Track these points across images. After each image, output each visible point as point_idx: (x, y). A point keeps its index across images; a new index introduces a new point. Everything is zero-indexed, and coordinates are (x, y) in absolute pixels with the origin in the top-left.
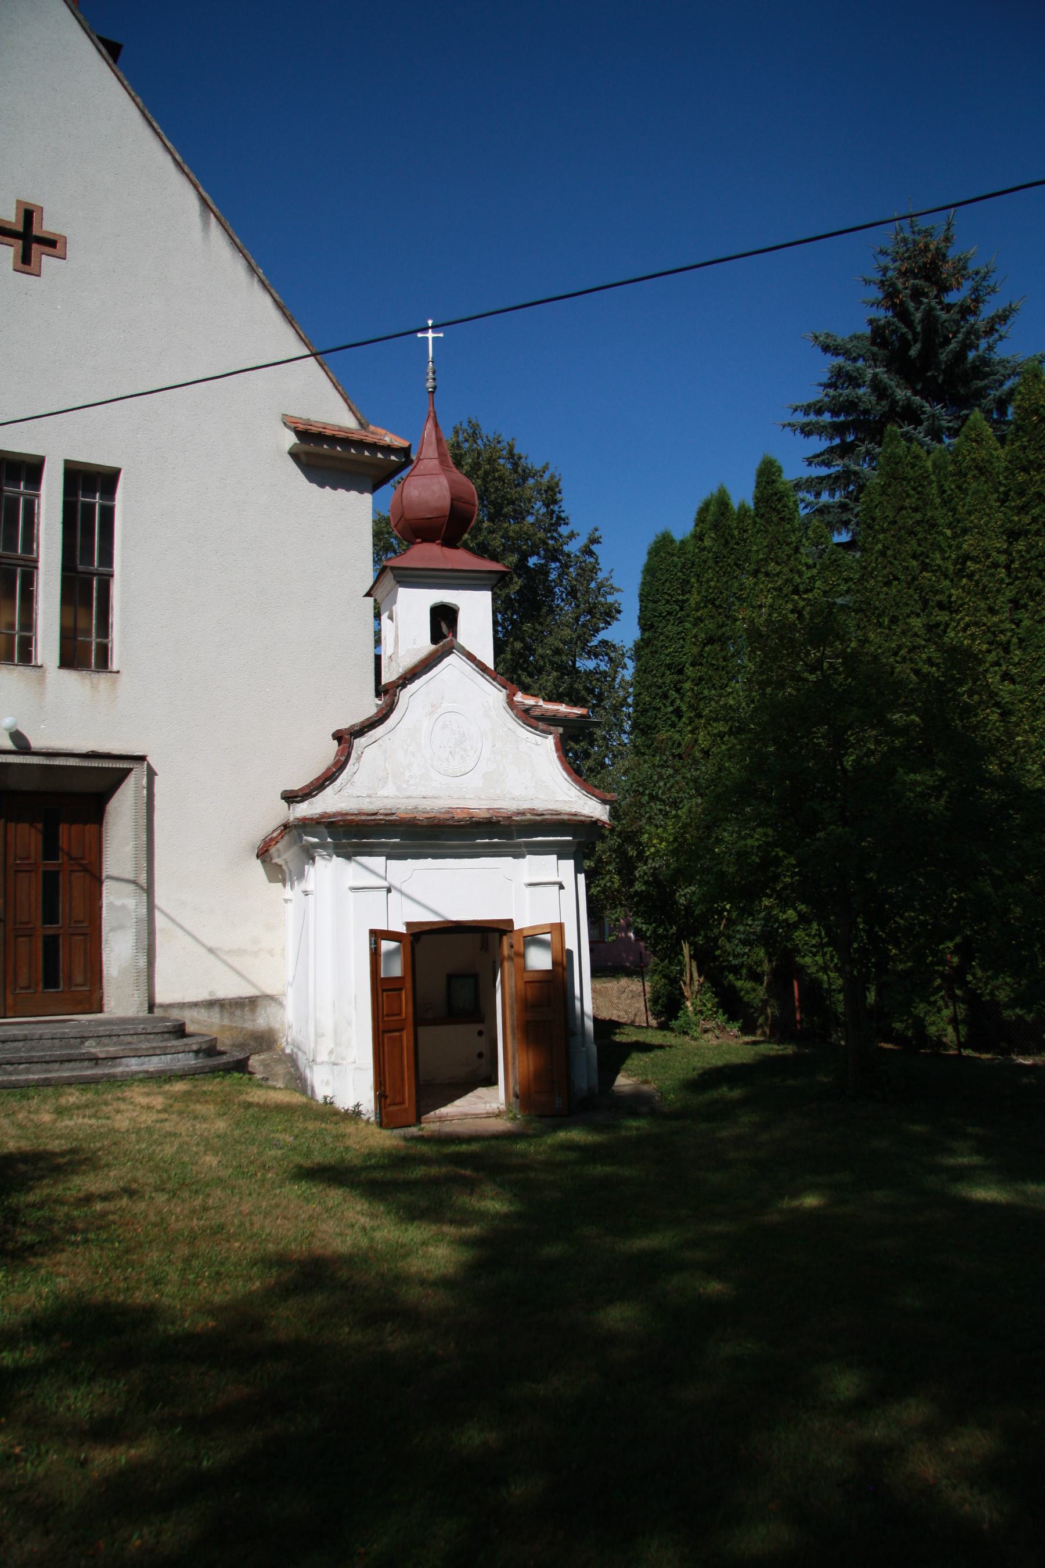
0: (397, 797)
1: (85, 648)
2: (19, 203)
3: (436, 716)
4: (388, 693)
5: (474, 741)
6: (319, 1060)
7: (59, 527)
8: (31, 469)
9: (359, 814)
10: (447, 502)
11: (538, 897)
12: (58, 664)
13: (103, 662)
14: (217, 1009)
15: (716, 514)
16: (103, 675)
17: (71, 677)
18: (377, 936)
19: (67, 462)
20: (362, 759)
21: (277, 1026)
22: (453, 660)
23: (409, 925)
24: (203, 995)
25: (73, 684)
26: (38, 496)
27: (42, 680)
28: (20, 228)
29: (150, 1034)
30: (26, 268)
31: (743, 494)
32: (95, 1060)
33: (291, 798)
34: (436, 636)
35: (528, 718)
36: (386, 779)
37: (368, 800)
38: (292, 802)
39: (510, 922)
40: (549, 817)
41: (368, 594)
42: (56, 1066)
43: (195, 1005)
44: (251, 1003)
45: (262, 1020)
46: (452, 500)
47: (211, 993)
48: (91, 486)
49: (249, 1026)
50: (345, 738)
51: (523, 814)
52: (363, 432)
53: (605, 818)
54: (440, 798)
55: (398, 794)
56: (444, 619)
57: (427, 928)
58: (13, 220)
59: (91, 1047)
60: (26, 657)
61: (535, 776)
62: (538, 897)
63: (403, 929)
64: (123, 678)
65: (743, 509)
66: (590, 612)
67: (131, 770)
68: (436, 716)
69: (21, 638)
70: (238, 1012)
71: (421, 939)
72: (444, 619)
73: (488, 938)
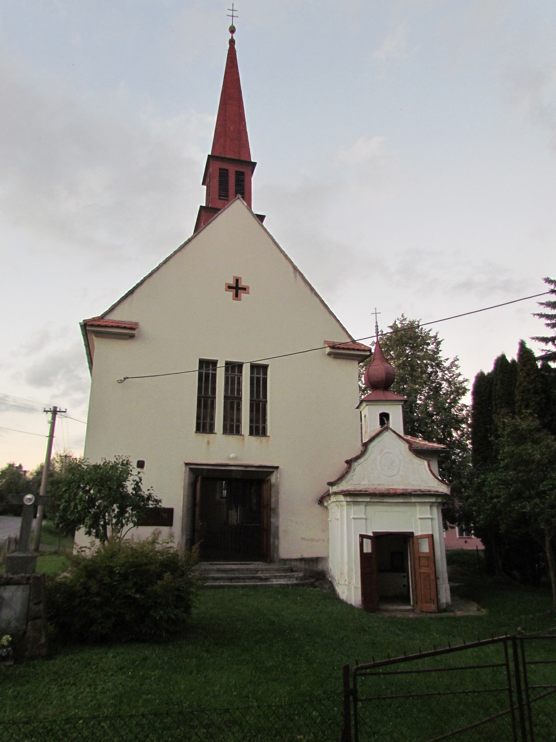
1: (259, 428)
4: (365, 445)
5: (398, 464)
6: (340, 583)
7: (249, 386)
9: (355, 491)
10: (384, 376)
11: (421, 522)
12: (248, 434)
14: (303, 562)
15: (501, 361)
16: (264, 438)
17: (253, 439)
18: (362, 537)
21: (325, 569)
22: (388, 435)
23: (373, 533)
24: (298, 556)
26: (242, 376)
27: (243, 439)
31: (512, 355)
32: (261, 579)
33: (331, 484)
34: (382, 423)
35: (419, 453)
36: (362, 478)
39: (412, 533)
41: (357, 408)
42: (248, 580)
43: (296, 560)
44: (316, 560)
45: (320, 567)
47: (301, 555)
48: (260, 371)
49: (315, 569)
50: (349, 463)
51: (416, 491)
52: (354, 345)
53: (448, 493)
56: (384, 418)
58: (242, 294)
59: (259, 574)
61: (423, 476)
62: (421, 522)
63: (371, 534)
64: (271, 439)
65: (513, 361)
67: (273, 472)
69: (236, 425)
70: (311, 563)
71: (379, 539)
72: (384, 418)
73: (405, 539)
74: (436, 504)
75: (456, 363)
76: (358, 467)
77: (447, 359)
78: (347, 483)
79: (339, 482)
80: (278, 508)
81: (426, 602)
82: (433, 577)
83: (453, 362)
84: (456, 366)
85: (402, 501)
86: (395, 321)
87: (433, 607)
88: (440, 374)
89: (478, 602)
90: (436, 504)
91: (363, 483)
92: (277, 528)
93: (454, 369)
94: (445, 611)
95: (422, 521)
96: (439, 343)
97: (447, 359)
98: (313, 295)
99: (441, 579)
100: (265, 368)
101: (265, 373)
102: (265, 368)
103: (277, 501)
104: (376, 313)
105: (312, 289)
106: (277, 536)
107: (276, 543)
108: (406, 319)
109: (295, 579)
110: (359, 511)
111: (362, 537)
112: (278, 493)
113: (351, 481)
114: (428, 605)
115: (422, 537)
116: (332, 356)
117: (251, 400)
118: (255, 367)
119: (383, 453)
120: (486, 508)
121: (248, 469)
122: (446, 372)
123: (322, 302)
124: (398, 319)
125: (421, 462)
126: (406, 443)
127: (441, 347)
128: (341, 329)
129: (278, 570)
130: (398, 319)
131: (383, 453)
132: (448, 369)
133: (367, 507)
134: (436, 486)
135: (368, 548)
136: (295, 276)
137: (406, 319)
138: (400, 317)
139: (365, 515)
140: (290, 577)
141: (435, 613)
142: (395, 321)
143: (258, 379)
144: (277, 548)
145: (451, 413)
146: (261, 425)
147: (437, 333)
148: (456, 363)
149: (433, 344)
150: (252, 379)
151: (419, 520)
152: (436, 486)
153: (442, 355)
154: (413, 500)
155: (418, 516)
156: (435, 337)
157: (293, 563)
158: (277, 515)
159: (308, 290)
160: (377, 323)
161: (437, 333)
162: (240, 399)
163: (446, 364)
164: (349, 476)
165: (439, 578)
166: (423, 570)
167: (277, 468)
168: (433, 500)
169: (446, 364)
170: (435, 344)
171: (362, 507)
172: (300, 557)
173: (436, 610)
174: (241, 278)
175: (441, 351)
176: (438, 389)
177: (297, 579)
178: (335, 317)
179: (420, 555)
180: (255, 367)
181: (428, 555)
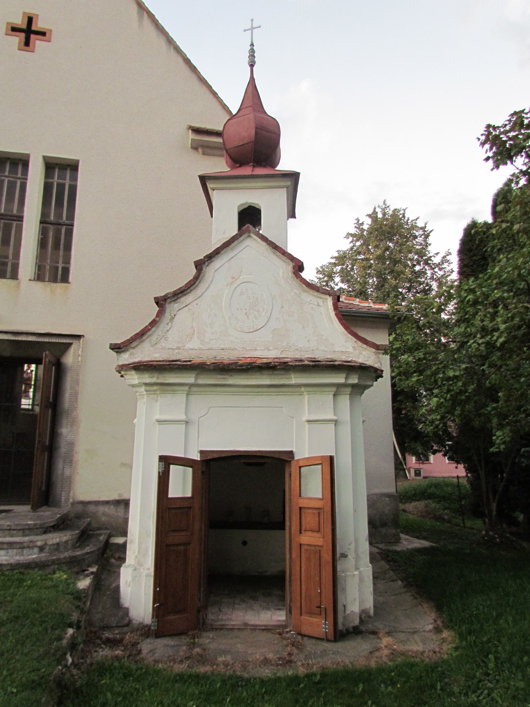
0: (200, 349)
2: (24, 13)
3: (235, 285)
8: (20, 162)
13: (65, 279)
18: (167, 461)
19: (44, 158)
20: (175, 319)
23: (202, 452)
25: (42, 290)
27: (18, 286)
28: (33, 36)
29: (14, 530)
30: (27, 48)
37: (177, 351)
38: (120, 352)
39: (291, 453)
40: (324, 363)
43: (107, 503)
46: (256, 128)
47: (120, 495)
48: (62, 172)
54: (236, 349)
55: (201, 346)
57: (216, 456)
58: (38, 42)
60: (14, 276)
63: (197, 457)
66: (440, 348)
68: (235, 285)
71: (214, 468)
73: (271, 468)
74: (349, 390)
75: (448, 258)
76: (182, 314)
77: (437, 254)
78: (152, 346)
79: (134, 344)
80: (75, 408)
81: (311, 613)
82: (327, 556)
83: (444, 257)
84: (448, 261)
85: (267, 382)
86: (375, 208)
87: (321, 625)
88: (429, 273)
89: (439, 608)
90: (349, 390)
91: (189, 346)
92: (71, 445)
93: (445, 265)
94: (356, 632)
95: (313, 425)
96: (427, 236)
97: (437, 254)
98: (172, 50)
99: (351, 557)
100: (72, 167)
101: (74, 178)
102: (72, 167)
103: (75, 395)
104: (252, 29)
105: (170, 41)
106: (70, 460)
107: (67, 472)
108: (388, 207)
109: (36, 550)
110: (170, 406)
111: (167, 461)
112: (77, 382)
113: (163, 344)
114: (314, 620)
115: (311, 462)
116: (200, 150)
117: (42, 222)
118: (51, 166)
119: (238, 282)
120: (451, 374)
121: (20, 338)
122: (436, 270)
123: (187, 61)
124: (379, 207)
125: (320, 301)
126: (288, 261)
127: (430, 240)
128: (220, 108)
129: (26, 530)
130: (379, 207)
131: (238, 282)
132: (438, 265)
133: (192, 398)
134: (351, 350)
135: (181, 484)
136: (141, 17)
137: (388, 207)
138: (381, 204)
139: (186, 413)
140: (21, 546)
141: (328, 641)
142: (375, 208)
143: (61, 187)
144: (69, 481)
145: (469, 386)
146: (60, 266)
147: (426, 224)
148: (448, 258)
149: (421, 237)
150: (47, 188)
151: (307, 425)
152: (351, 350)
153: (432, 250)
154: (295, 379)
155: (306, 417)
156: (423, 229)
157: (101, 509)
158: (74, 422)
159: (162, 41)
160: (252, 45)
161: (426, 224)
162: (20, 218)
163: (437, 260)
164: (157, 333)
165: (344, 556)
166: (307, 538)
167: (78, 337)
168: (339, 379)
169: (437, 260)
170: (423, 237)
171: (180, 398)
172: (117, 498)
173: (331, 637)
174: (37, 16)
175: (430, 244)
176: (426, 291)
177: (41, 549)
178: (209, 87)
179: (303, 503)
180: (51, 166)
181: (319, 504)
